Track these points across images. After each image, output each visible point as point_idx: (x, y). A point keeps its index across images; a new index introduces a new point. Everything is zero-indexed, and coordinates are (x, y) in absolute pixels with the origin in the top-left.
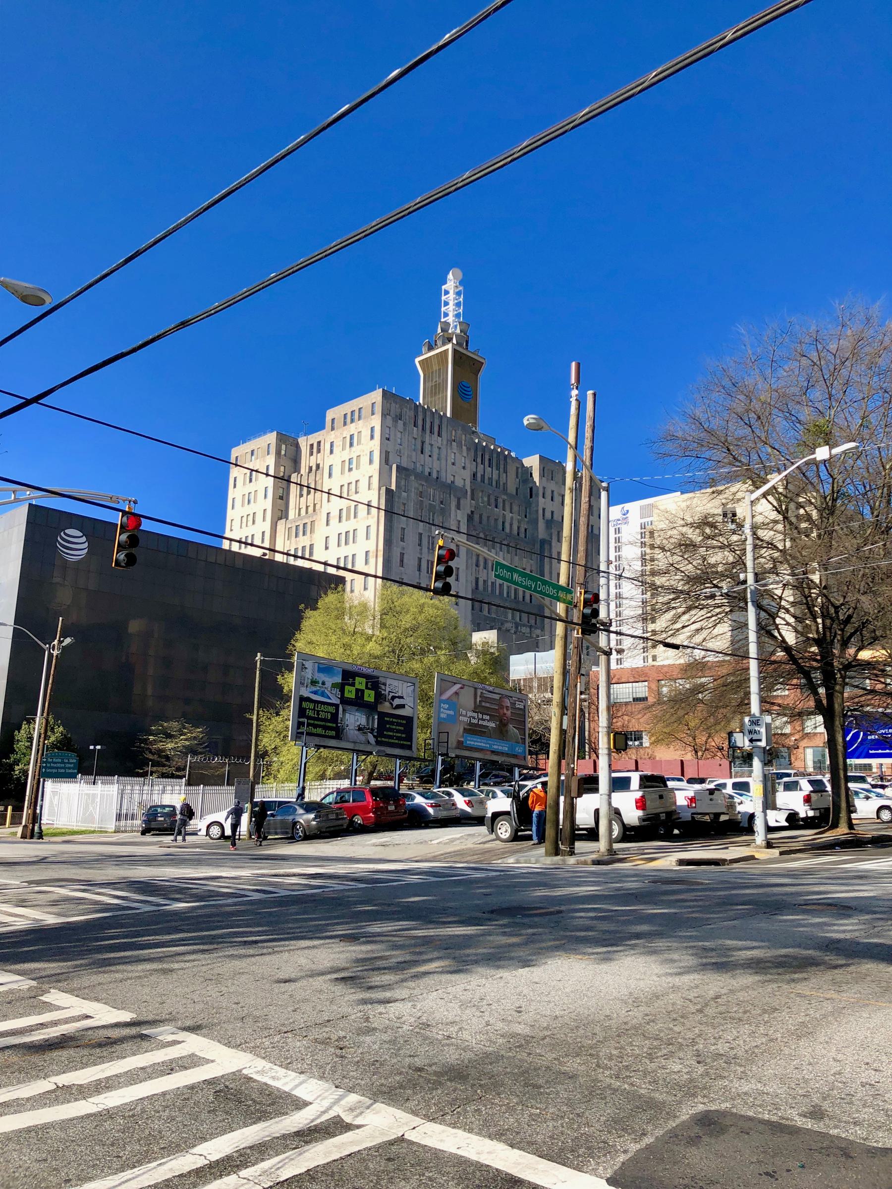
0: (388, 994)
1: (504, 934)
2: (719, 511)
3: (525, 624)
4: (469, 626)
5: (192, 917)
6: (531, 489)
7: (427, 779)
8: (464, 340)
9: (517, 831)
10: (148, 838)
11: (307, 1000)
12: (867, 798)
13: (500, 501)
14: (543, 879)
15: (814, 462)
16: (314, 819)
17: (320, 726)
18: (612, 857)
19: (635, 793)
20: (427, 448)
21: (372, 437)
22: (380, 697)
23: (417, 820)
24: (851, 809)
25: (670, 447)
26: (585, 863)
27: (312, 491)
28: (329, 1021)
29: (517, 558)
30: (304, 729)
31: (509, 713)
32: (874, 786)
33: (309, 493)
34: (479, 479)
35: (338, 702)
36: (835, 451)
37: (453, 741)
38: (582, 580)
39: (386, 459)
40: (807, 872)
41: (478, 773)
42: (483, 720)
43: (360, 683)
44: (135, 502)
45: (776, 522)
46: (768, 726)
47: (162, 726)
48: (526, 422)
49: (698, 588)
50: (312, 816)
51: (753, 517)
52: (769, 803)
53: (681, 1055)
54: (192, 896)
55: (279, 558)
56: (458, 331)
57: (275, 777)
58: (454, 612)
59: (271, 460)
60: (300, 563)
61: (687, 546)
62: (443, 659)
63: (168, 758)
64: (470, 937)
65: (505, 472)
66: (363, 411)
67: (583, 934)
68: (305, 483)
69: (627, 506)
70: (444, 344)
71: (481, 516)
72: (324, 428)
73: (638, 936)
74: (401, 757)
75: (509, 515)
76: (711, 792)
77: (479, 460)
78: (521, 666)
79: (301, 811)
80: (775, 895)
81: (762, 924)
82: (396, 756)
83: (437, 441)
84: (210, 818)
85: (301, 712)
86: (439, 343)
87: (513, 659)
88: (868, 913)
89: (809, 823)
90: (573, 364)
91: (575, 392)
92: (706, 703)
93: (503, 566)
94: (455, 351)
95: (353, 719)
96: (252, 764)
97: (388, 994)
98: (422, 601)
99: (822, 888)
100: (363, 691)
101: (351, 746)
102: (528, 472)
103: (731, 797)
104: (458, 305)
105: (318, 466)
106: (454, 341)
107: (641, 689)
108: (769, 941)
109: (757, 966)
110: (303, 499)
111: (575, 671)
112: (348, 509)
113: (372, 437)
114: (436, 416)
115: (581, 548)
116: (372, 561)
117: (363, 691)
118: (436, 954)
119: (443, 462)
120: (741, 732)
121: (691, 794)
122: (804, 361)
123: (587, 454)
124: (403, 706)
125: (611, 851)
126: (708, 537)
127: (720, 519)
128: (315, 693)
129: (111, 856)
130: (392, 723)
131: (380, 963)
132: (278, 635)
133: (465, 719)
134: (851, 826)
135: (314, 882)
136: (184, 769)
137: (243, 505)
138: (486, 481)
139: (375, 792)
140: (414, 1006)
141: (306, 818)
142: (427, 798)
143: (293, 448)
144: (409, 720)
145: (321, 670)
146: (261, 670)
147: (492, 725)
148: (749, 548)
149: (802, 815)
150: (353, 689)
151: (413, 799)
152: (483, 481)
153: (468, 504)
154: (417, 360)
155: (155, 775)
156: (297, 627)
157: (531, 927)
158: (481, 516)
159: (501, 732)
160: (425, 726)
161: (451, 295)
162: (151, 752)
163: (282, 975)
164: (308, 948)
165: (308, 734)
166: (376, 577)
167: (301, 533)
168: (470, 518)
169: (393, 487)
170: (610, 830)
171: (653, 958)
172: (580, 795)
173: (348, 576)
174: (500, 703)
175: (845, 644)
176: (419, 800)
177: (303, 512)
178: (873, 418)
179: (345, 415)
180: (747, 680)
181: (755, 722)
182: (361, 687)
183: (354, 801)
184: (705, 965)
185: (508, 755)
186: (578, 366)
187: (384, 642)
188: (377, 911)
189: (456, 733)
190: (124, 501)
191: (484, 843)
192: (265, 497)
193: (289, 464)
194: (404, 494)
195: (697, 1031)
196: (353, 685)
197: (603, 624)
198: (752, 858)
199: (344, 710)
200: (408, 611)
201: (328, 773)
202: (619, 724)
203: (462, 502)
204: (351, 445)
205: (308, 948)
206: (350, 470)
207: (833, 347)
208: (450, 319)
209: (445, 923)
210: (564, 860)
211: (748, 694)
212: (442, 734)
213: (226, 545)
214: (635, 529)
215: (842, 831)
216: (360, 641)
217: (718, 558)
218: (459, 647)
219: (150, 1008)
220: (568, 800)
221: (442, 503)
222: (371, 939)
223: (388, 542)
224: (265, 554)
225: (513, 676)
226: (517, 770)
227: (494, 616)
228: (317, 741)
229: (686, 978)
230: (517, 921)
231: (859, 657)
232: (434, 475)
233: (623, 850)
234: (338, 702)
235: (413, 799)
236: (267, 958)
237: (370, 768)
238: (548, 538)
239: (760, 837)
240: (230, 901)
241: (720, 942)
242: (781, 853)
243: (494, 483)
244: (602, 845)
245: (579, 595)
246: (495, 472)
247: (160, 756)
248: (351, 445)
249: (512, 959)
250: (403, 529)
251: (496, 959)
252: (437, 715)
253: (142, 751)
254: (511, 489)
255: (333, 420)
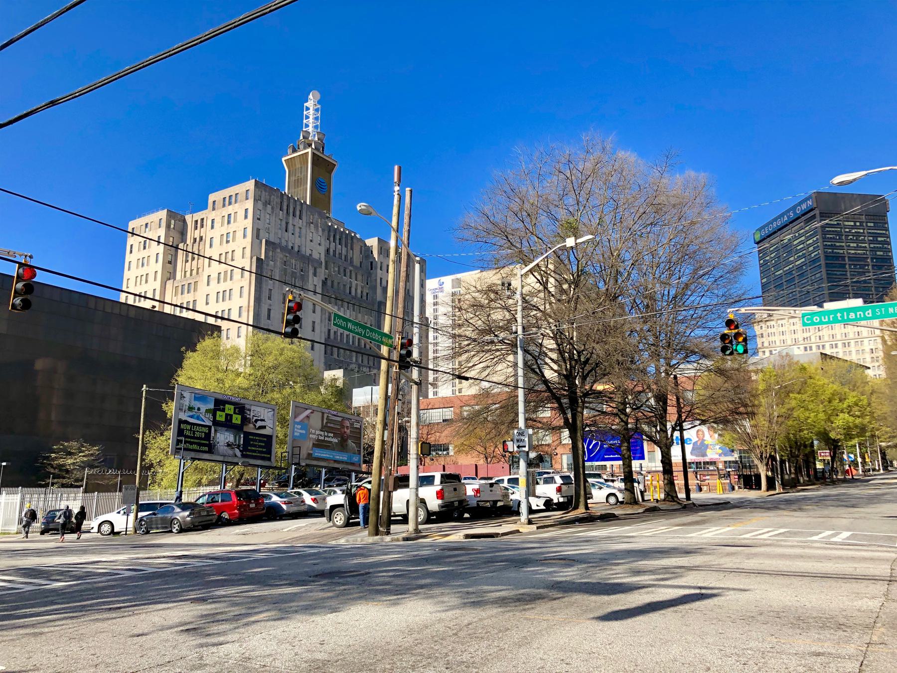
0: (222, 639)
1: (323, 590)
2: (500, 282)
3: (361, 362)
4: (322, 365)
5: (69, 593)
6: (372, 263)
7: (283, 484)
8: (321, 146)
9: (349, 519)
10: (47, 537)
11: (155, 648)
12: (600, 488)
13: (348, 271)
14: (362, 552)
15: (564, 248)
16: (188, 516)
17: (195, 443)
18: (418, 534)
19: (437, 486)
20: (290, 227)
21: (246, 217)
22: (245, 420)
23: (274, 514)
24: (588, 496)
25: (467, 234)
26: (398, 540)
27: (196, 256)
28: (169, 662)
29: (360, 315)
30: (182, 446)
31: (348, 431)
32: (606, 481)
33: (193, 259)
34: (331, 253)
35: (210, 424)
36: (579, 241)
37: (304, 453)
38: (400, 330)
39: (257, 234)
40: (552, 539)
41: (323, 477)
42: (328, 437)
43: (229, 409)
44: (31, 257)
45: (539, 291)
46: (530, 437)
47: (62, 445)
48: (359, 208)
49: (488, 338)
50: (187, 513)
51: (523, 287)
52: (530, 492)
53: (436, 664)
54: (70, 576)
55: (168, 309)
56: (316, 139)
57: (159, 485)
58: (308, 354)
59: (162, 232)
60: (186, 314)
61: (477, 306)
62: (298, 391)
63: (67, 471)
64: (295, 594)
65: (352, 249)
66: (239, 196)
67: (381, 587)
68: (190, 249)
69: (443, 279)
70: (305, 148)
71: (332, 282)
72: (206, 208)
73: (421, 587)
74: (262, 467)
75: (354, 283)
76: (492, 485)
77: (332, 239)
78: (361, 397)
79: (178, 510)
80: (525, 554)
81: (512, 574)
82: (258, 466)
83: (298, 223)
84: (102, 518)
85: (180, 432)
86: (301, 147)
87: (355, 391)
88: (585, 563)
89: (560, 507)
90: (396, 168)
91: (397, 188)
92: (490, 421)
93: (340, 317)
94: (314, 154)
95: (223, 438)
96: (138, 475)
97: (222, 639)
98: (282, 345)
99: (559, 549)
100: (231, 416)
101: (221, 459)
102: (368, 251)
103: (506, 489)
104: (316, 119)
105: (201, 238)
106: (313, 146)
107: (449, 414)
108: (514, 585)
109: (502, 602)
110: (188, 264)
111: (396, 400)
112: (226, 272)
113: (246, 217)
114: (298, 203)
115: (401, 305)
116: (244, 314)
117: (231, 416)
118: (266, 608)
119: (303, 239)
120: (512, 440)
121: (477, 487)
122: (562, 176)
123: (405, 234)
124: (264, 427)
125: (417, 530)
126: (492, 300)
127: (500, 287)
128: (191, 417)
129: (6, 551)
130: (255, 440)
131: (220, 617)
132: (163, 373)
133: (314, 436)
134: (587, 508)
135: (178, 561)
136: (82, 480)
137: (137, 267)
138: (337, 255)
139: (239, 494)
140: (241, 646)
141: (183, 515)
142: (281, 497)
143: (181, 223)
144: (269, 438)
145: (196, 399)
146: (146, 399)
147: (335, 440)
148: (519, 308)
149: (555, 501)
150: (223, 414)
151: (270, 499)
152: (334, 255)
153: (322, 273)
154: (283, 159)
155: (56, 486)
156: (180, 365)
157: (343, 585)
158: (332, 282)
159: (342, 446)
160: (282, 443)
161: (311, 111)
162: (52, 467)
163: (136, 632)
164: (164, 609)
165: (185, 449)
166: (248, 325)
167: (186, 291)
168: (324, 283)
169: (263, 257)
170: (417, 516)
171: (430, 601)
172: (395, 489)
173: (224, 325)
174: (341, 424)
175: (584, 378)
176: (275, 499)
177: (188, 274)
178: (607, 219)
179: (224, 198)
180: (517, 403)
181: (521, 434)
182: (230, 412)
183: (222, 501)
184: (465, 604)
185: (347, 463)
186: (400, 169)
187: (251, 378)
188: (225, 580)
189: (307, 447)
190: (21, 255)
191: (324, 529)
192: (157, 261)
193: (178, 236)
194: (271, 263)
195: (450, 648)
196: (223, 410)
197: (415, 362)
198: (518, 531)
199: (216, 431)
200: (271, 353)
201: (203, 481)
202: (433, 439)
203: (318, 270)
204: (229, 222)
205: (164, 609)
206: (228, 242)
207: (581, 168)
208: (310, 129)
209: (277, 585)
210: (382, 540)
211: (517, 415)
212: (295, 449)
213: (122, 298)
214: (440, 294)
215: (580, 511)
216: (231, 376)
217: (498, 316)
218: (312, 383)
219: (18, 662)
220: (386, 494)
221: (302, 271)
222: (216, 600)
223: (258, 300)
224: (154, 307)
225: (355, 404)
226: (353, 474)
227: (342, 359)
228: (193, 455)
229: (450, 613)
230: (334, 581)
231: (594, 388)
232: (296, 249)
233: (427, 529)
234: (210, 424)
235: (270, 498)
236: (127, 619)
237: (238, 476)
238: (383, 300)
239: (524, 517)
240: (104, 579)
241: (480, 588)
242: (538, 528)
243: (343, 257)
244: (411, 526)
245: (397, 340)
246: (344, 249)
247: (60, 470)
248: (229, 222)
249: (325, 607)
250: (270, 290)
251: (311, 608)
252: (291, 432)
253: (44, 466)
254: (357, 262)
255: (214, 202)
